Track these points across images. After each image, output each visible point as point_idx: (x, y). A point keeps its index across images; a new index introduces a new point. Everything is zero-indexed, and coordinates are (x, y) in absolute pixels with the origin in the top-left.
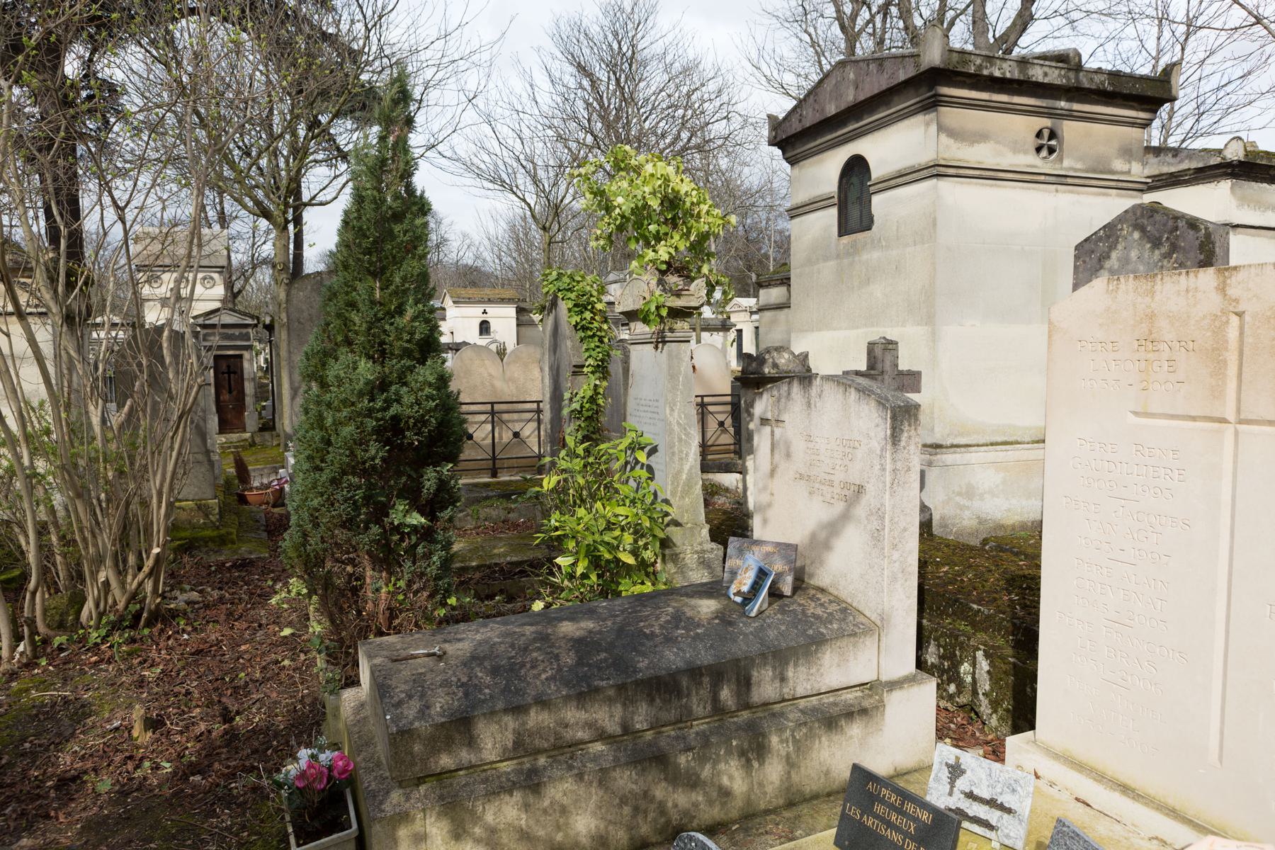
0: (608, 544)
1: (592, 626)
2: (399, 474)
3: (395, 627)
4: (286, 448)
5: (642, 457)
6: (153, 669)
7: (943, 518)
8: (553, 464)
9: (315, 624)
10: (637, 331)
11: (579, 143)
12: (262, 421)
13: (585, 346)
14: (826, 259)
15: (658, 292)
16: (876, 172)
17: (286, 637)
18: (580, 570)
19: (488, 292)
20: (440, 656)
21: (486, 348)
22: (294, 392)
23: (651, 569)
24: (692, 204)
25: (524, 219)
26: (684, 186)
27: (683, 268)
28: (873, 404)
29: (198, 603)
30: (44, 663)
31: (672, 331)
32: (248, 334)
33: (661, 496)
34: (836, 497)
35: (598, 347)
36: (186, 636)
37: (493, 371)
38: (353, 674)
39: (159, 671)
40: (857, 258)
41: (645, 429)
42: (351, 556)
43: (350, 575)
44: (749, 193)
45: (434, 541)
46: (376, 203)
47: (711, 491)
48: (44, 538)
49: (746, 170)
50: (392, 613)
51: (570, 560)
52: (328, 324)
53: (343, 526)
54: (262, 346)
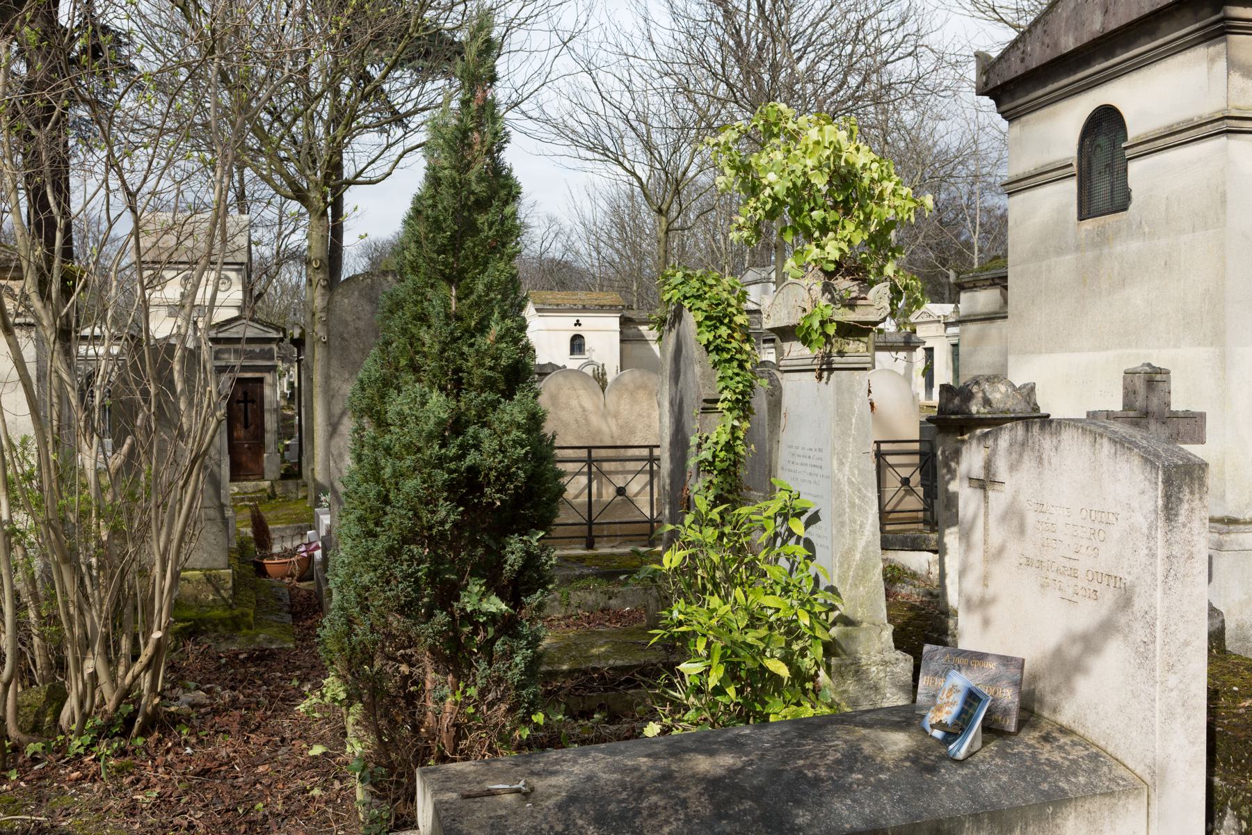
0: (751, 646)
1: (731, 761)
2: (474, 543)
3: (462, 751)
4: (317, 502)
5: (797, 526)
6: (148, 792)
7: (1240, 627)
8: (674, 535)
9: (354, 741)
10: (793, 354)
11: (709, 95)
12: (284, 466)
13: (719, 374)
14: (1060, 251)
15: (823, 302)
16: (1136, 128)
17: (315, 757)
18: (713, 681)
19: (582, 296)
20: (526, 794)
21: (579, 372)
22: (333, 428)
23: (809, 685)
24: (872, 180)
25: (632, 197)
26: (861, 157)
27: (858, 269)
28: (1136, 461)
29: (204, 706)
30: (14, 777)
31: (841, 353)
32: (271, 350)
33: (824, 583)
34: (1081, 592)
35: (737, 375)
36: (189, 750)
37: (588, 404)
38: (405, 812)
39: (155, 795)
40: (1106, 251)
41: (803, 488)
42: (409, 651)
43: (405, 678)
44: (944, 159)
45: (517, 636)
46: (455, 187)
47: (893, 576)
48: (22, 614)
49: (941, 126)
50: (460, 731)
51: (698, 667)
52: (388, 343)
53: (401, 610)
54: (286, 366)
